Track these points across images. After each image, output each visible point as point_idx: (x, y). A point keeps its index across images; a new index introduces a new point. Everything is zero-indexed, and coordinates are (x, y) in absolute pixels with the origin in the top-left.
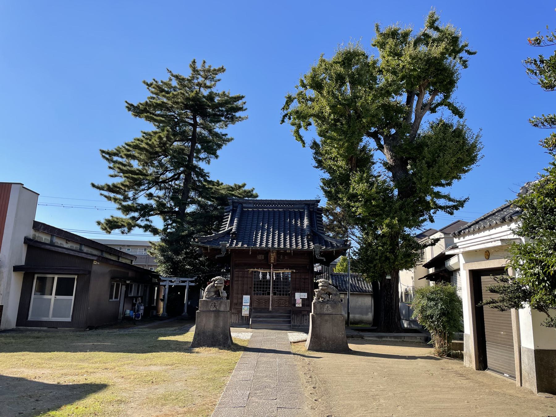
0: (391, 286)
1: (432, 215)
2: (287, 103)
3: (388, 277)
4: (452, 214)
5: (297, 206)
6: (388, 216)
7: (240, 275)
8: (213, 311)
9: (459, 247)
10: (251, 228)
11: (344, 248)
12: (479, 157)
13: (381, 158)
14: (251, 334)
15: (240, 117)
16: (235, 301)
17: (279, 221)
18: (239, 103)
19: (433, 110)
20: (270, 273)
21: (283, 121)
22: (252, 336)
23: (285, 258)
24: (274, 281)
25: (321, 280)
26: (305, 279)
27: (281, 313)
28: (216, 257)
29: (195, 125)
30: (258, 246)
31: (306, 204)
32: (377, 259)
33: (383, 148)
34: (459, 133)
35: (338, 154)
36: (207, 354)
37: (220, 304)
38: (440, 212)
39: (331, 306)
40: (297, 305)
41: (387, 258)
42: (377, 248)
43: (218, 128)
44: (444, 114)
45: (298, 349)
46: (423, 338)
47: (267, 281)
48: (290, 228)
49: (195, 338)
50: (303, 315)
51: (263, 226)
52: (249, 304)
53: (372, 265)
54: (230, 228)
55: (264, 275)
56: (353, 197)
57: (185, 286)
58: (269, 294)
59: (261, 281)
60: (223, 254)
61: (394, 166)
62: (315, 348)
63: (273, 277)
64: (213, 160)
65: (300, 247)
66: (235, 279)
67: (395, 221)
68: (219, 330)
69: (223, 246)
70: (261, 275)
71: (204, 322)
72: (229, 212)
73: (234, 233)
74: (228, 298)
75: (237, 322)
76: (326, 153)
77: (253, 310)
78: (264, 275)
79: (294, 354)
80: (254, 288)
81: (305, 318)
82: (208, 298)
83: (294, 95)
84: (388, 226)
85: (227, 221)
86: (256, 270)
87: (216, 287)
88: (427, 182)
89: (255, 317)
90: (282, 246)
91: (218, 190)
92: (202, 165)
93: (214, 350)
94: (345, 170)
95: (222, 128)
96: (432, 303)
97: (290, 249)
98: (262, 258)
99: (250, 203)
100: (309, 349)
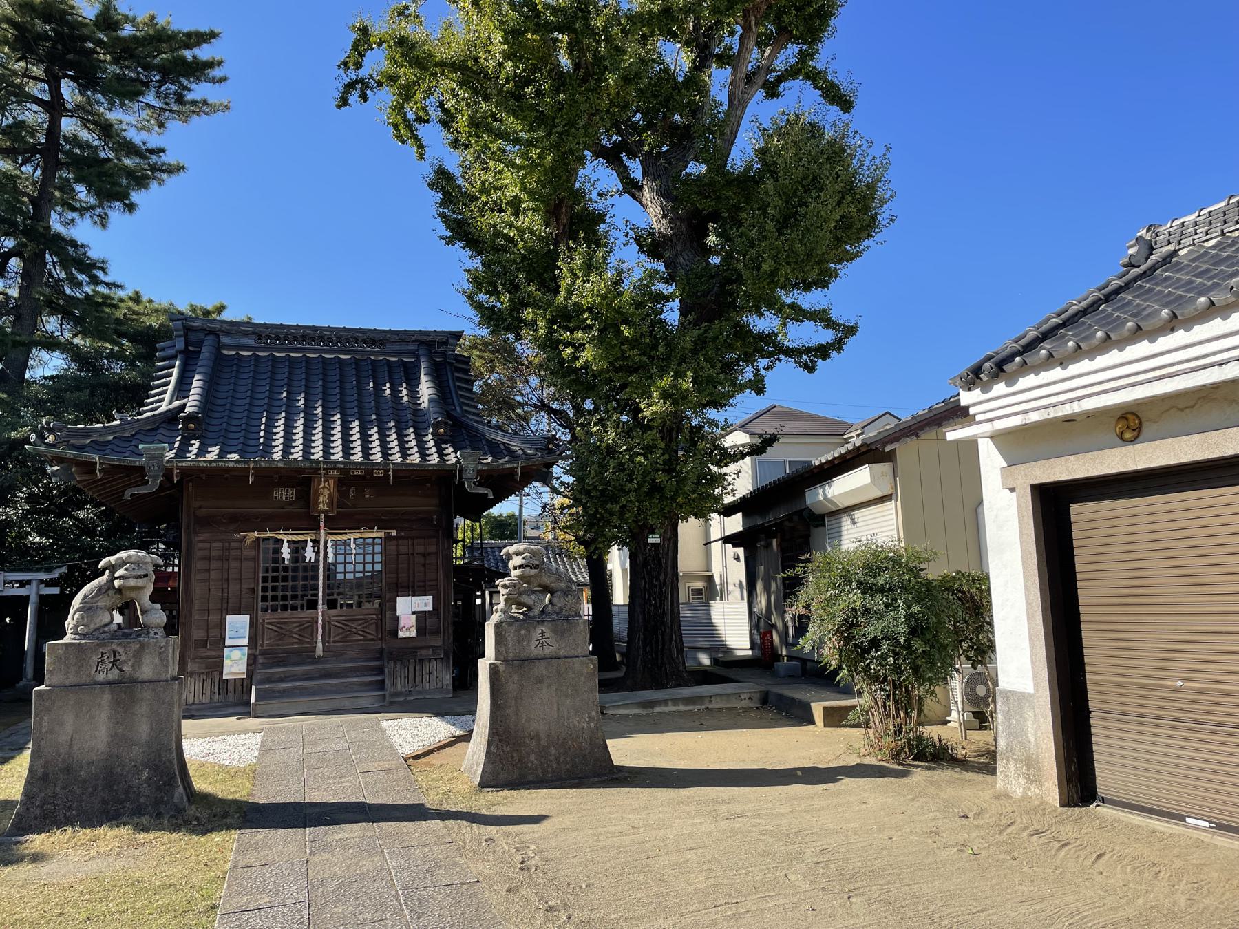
0: (660, 561)
1: (763, 372)
2: (355, 47)
3: (654, 539)
4: (810, 369)
5: (396, 347)
6: (663, 371)
7: (215, 553)
8: (110, 683)
9: (978, 418)
10: (251, 405)
11: (548, 459)
12: (883, 218)
13: (632, 213)
14: (259, 737)
15: (205, 103)
16: (198, 635)
17: (342, 388)
18: (204, 53)
19: (772, 91)
20: (316, 542)
21: (344, 101)
22: (264, 749)
23: (364, 495)
24: (328, 568)
25: (521, 547)
26: (424, 555)
27: (353, 660)
28: (127, 495)
29: (55, 107)
30: (277, 456)
31: (421, 343)
32: (629, 491)
33: (641, 188)
34: (837, 153)
35: (524, 189)
36: (81, 858)
37: (138, 656)
38: (786, 366)
39: (554, 631)
40: (401, 634)
41: (656, 488)
42: (632, 460)
43: (130, 120)
44: (801, 99)
45: (442, 787)
46: (756, 697)
47: (306, 568)
48: (377, 408)
49: (28, 793)
50: (421, 661)
51: (291, 399)
52: (246, 641)
53: (616, 508)
54: (176, 404)
55: (297, 548)
56: (567, 317)
57: (28, 597)
58: (313, 605)
59: (286, 569)
60: (153, 485)
61: (670, 239)
62: (503, 776)
63: (326, 553)
64: (116, 215)
65: (415, 458)
66: (199, 565)
67: (687, 384)
68: (136, 753)
69: (151, 457)
70: (286, 552)
71: (69, 728)
72: (174, 357)
73: (191, 418)
74: (170, 629)
75: (206, 699)
76: (482, 191)
77: (261, 660)
78: (297, 548)
79: (444, 815)
80: (265, 589)
81: (426, 670)
82: (84, 636)
83: (380, 27)
84: (665, 395)
85: (167, 384)
86: (269, 534)
87: (119, 591)
88: (774, 273)
89: (268, 680)
90: (358, 457)
91: (137, 313)
92: (83, 231)
93: (111, 836)
94: (540, 239)
95: (148, 130)
96: (880, 600)
97: (385, 466)
98: (293, 494)
99: (245, 334)
100: (483, 785)
